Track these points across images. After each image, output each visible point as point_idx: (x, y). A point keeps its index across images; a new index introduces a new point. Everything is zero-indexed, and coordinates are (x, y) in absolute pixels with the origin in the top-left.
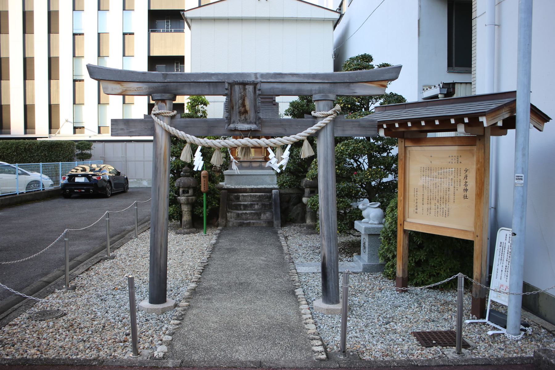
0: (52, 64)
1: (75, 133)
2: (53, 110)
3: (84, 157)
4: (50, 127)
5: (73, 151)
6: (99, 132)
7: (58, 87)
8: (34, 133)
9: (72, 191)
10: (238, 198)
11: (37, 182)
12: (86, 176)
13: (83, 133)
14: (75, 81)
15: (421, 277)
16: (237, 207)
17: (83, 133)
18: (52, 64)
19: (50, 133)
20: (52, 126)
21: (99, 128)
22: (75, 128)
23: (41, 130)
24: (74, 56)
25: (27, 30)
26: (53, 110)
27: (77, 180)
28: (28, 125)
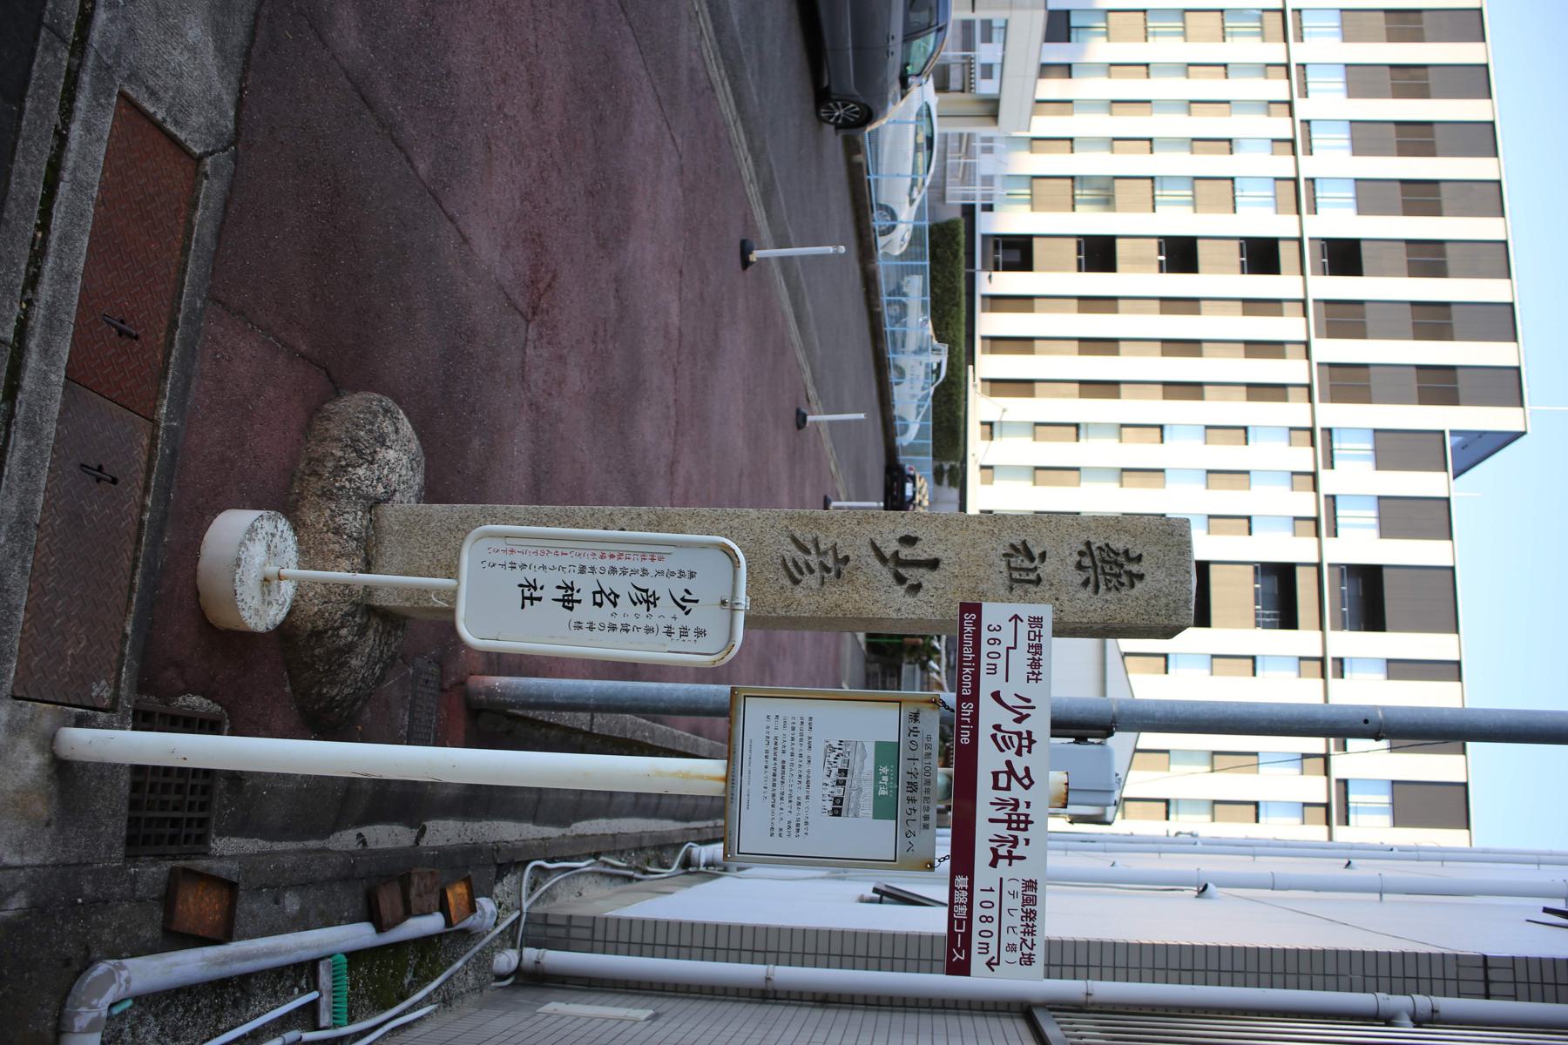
0: (1110, 388)
1: (983, 423)
2: (1024, 386)
3: (938, 475)
4: (993, 381)
5: (948, 460)
6: (983, 467)
7: (1064, 396)
8: (983, 310)
9: (894, 479)
10: (892, 676)
11: (906, 429)
12: (914, 497)
13: (983, 438)
14: (1077, 426)
15: (717, 803)
16: (884, 675)
17: (983, 438)
18: (1110, 388)
19: (983, 380)
20: (999, 386)
21: (991, 467)
22: (991, 424)
23: (988, 365)
24: (1123, 426)
25: (1169, 388)
26: (1024, 386)
27: (909, 486)
28: (999, 302)
